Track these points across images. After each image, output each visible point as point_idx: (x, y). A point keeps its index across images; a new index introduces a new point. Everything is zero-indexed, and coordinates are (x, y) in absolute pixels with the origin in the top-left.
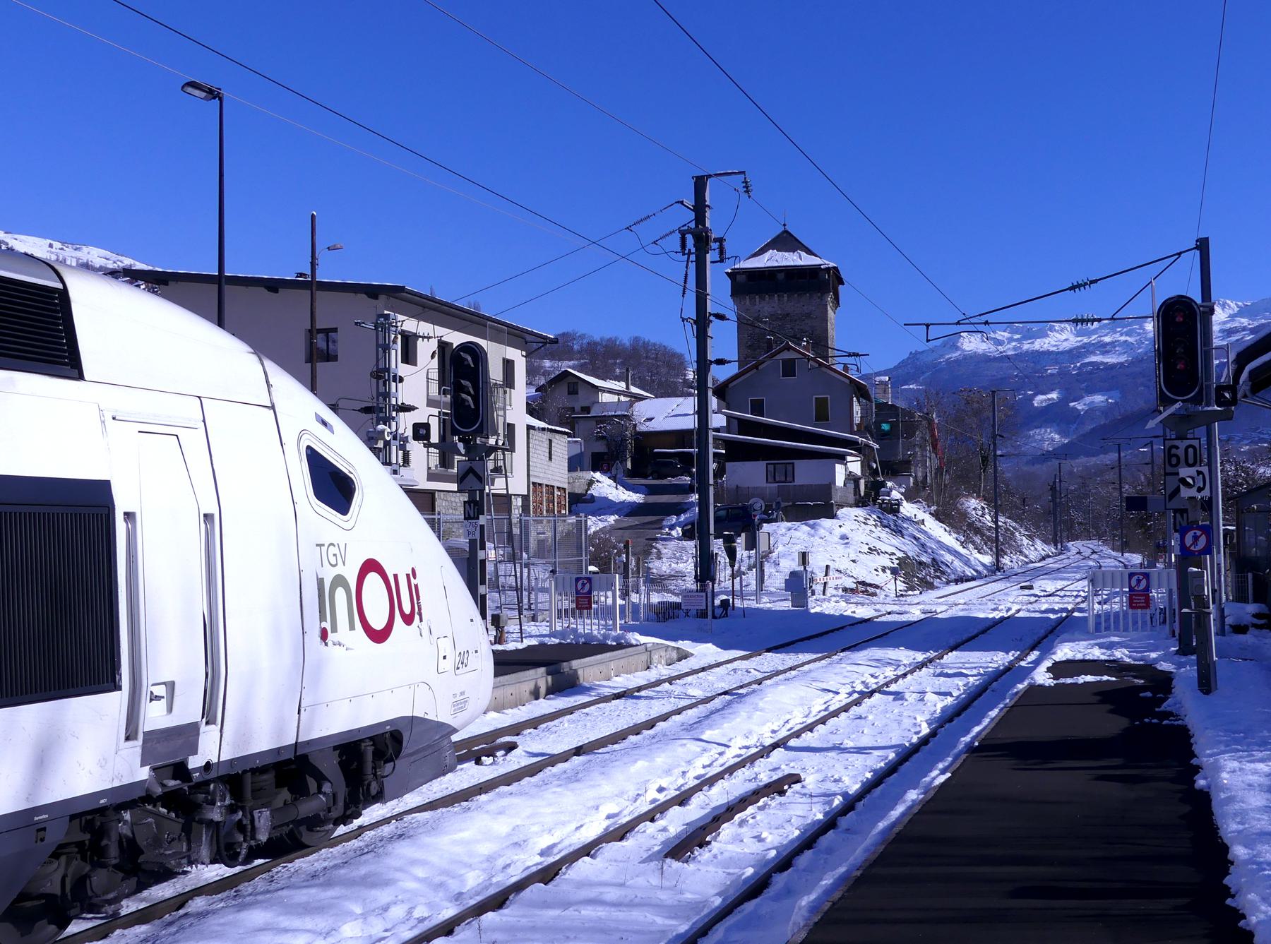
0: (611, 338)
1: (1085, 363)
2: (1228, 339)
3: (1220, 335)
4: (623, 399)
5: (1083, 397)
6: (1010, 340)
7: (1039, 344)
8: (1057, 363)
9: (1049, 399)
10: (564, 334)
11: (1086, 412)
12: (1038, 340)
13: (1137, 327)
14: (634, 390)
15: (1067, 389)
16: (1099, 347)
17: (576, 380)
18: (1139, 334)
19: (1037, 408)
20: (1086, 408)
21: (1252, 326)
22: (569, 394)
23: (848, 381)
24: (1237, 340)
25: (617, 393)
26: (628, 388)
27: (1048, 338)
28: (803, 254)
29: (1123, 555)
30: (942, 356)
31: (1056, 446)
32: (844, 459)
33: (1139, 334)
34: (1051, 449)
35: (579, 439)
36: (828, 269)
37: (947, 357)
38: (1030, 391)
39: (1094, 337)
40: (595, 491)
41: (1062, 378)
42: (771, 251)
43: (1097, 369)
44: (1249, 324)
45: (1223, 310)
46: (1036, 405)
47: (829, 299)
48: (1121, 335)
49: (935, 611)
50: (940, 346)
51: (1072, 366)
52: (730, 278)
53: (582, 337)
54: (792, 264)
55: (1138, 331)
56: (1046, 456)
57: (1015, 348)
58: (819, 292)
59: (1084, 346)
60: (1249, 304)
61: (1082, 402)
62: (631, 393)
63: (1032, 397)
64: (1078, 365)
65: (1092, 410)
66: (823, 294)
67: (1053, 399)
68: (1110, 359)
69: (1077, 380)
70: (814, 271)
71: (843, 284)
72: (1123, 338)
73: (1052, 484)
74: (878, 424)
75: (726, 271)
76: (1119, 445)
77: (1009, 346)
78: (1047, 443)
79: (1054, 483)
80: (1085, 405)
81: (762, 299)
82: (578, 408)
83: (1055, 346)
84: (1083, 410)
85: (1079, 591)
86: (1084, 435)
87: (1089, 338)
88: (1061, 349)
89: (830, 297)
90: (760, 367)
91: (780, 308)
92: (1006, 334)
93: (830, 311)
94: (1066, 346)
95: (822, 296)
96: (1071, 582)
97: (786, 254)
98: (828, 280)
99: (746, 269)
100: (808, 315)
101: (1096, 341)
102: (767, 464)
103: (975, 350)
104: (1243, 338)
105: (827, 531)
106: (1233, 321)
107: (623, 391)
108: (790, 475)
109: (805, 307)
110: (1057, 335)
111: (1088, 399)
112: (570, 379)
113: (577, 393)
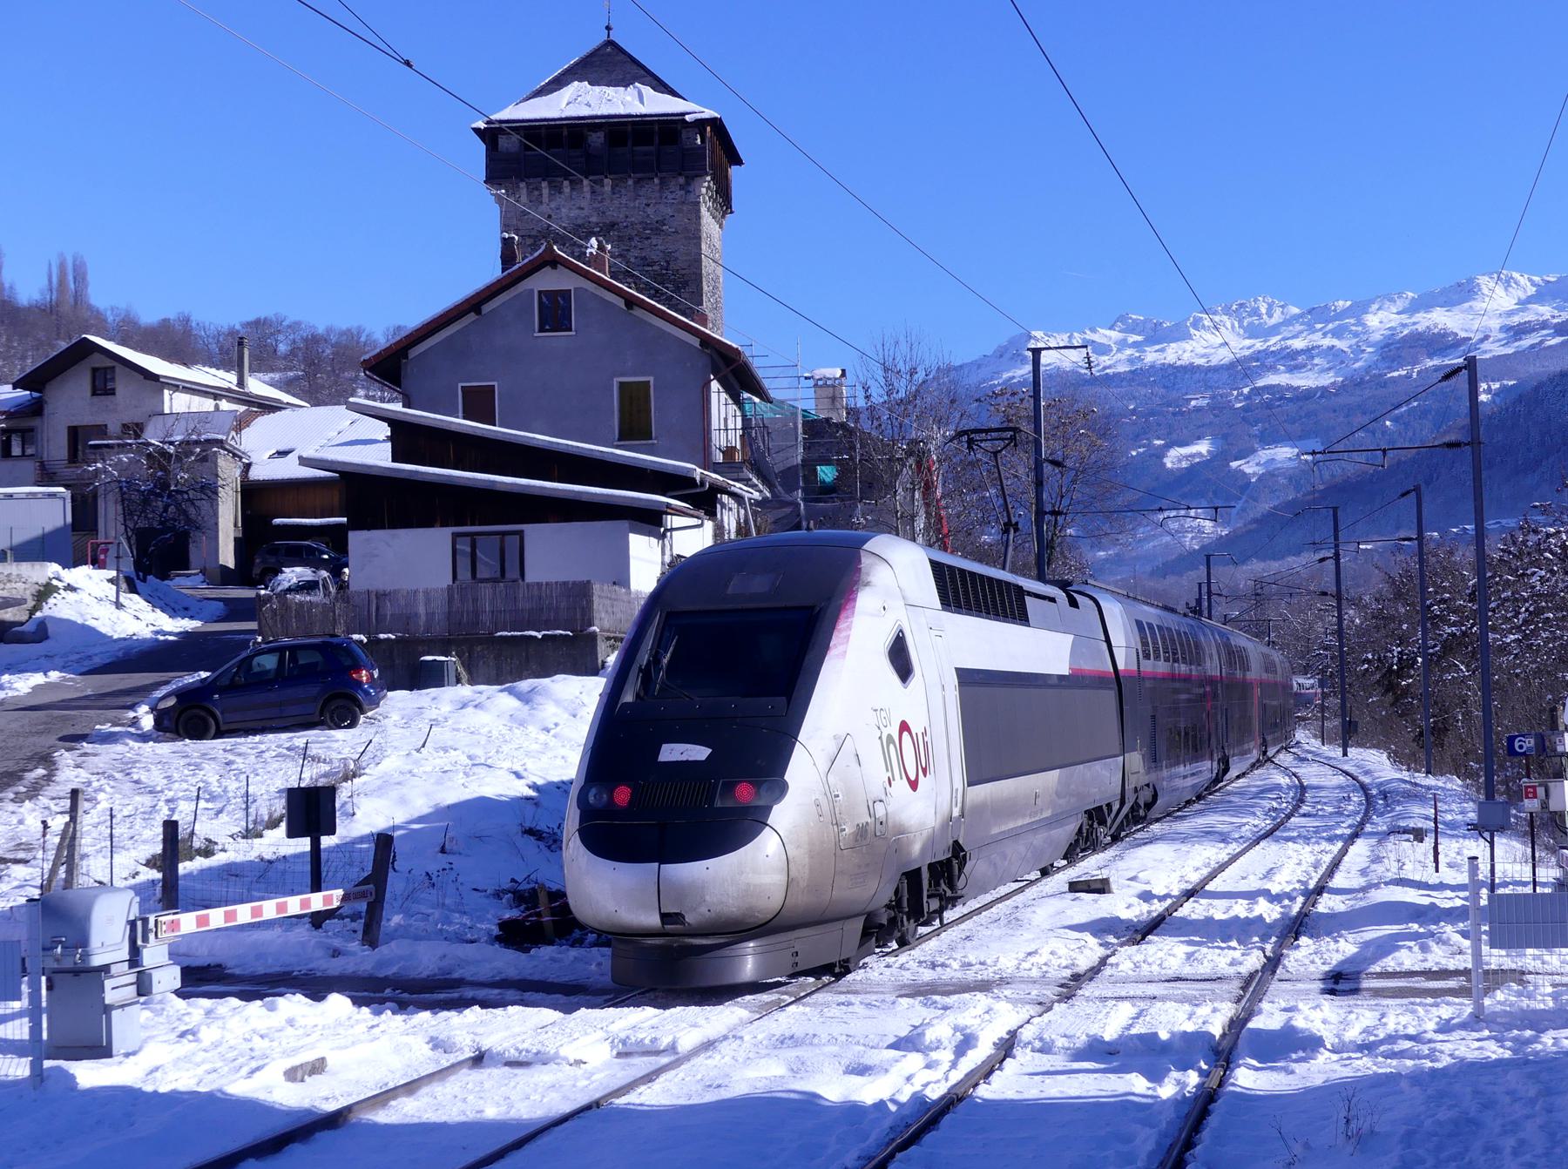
0: (349, 330)
1: (1260, 388)
2: (1516, 344)
3: (1503, 335)
4: (225, 405)
5: (1254, 451)
6: (1123, 345)
7: (1175, 353)
8: (1208, 387)
9: (1193, 456)
10: (257, 323)
11: (1261, 478)
12: (1173, 345)
13: (1352, 321)
14: (257, 386)
15: (1225, 437)
16: (1282, 358)
17: (109, 363)
18: (1356, 335)
19: (1172, 470)
20: (1261, 470)
21: (1559, 320)
22: (94, 394)
23: (695, 342)
24: (1532, 346)
25: (215, 394)
26: (241, 383)
27: (1191, 342)
28: (647, 91)
29: (1345, 754)
30: (998, 373)
31: (1206, 541)
32: (660, 523)
33: (1356, 335)
34: (1197, 547)
35: (62, 489)
36: (701, 124)
37: (1005, 376)
38: (1159, 438)
39: (1274, 340)
40: (60, 608)
41: (1215, 416)
42: (576, 83)
43: (1281, 398)
44: (1553, 317)
45: (1506, 290)
46: (1169, 465)
47: (704, 190)
48: (1325, 335)
49: (672, 1048)
50: (991, 356)
51: (1235, 393)
52: (483, 140)
53: (295, 326)
54: (622, 111)
55: (1354, 328)
56: (1185, 561)
57: (1131, 361)
58: (680, 174)
59: (1258, 356)
60: (1553, 279)
61: (1254, 459)
62: (247, 394)
63: (1160, 454)
64: (1246, 390)
65: (1270, 476)
66: (690, 179)
67: (1200, 454)
68: (1305, 381)
69: (1244, 419)
70: (670, 127)
71: (739, 162)
72: (1327, 342)
73: (1194, 605)
74: (809, 466)
75: (474, 126)
76: (1335, 509)
77: (1119, 356)
78: (1190, 535)
79: (1199, 601)
80: (1257, 464)
81: (556, 189)
82: (114, 427)
83: (1203, 356)
84: (1254, 474)
85: (1251, 896)
86: (1256, 521)
87: (1265, 341)
88: (1214, 362)
89: (705, 188)
90: (486, 308)
91: (597, 209)
92: (1115, 335)
93: (708, 223)
94: (1223, 356)
95: (688, 183)
96: (1234, 848)
97: (610, 91)
98: (702, 148)
99: (523, 121)
100: (657, 229)
101: (1278, 347)
102: (455, 536)
103: (1058, 363)
104: (1542, 342)
105: (566, 709)
106: (1523, 310)
107: (229, 390)
108: (511, 563)
109: (650, 211)
110: (1208, 336)
111: (1264, 454)
112: (98, 361)
113: (112, 392)
